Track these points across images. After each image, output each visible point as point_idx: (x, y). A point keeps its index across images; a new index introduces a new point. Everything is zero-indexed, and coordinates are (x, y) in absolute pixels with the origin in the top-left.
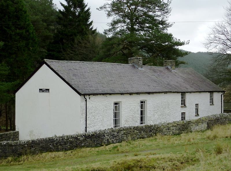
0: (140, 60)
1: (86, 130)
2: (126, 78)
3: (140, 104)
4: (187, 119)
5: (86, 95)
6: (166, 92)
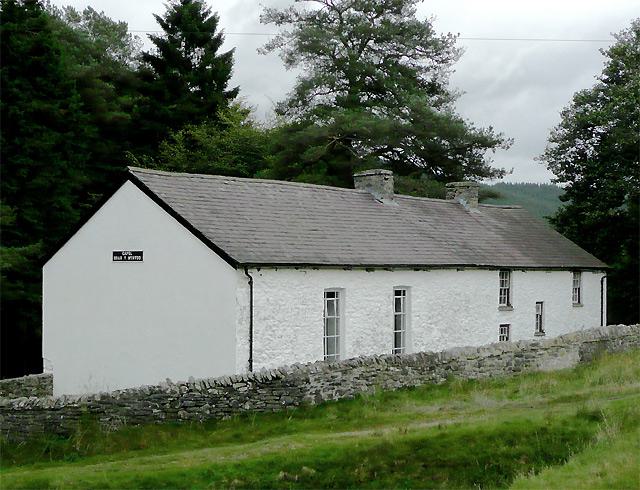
0: (386, 179)
1: (251, 365)
2: (353, 226)
3: (393, 298)
4: (515, 336)
5: (252, 267)
6: (460, 267)
